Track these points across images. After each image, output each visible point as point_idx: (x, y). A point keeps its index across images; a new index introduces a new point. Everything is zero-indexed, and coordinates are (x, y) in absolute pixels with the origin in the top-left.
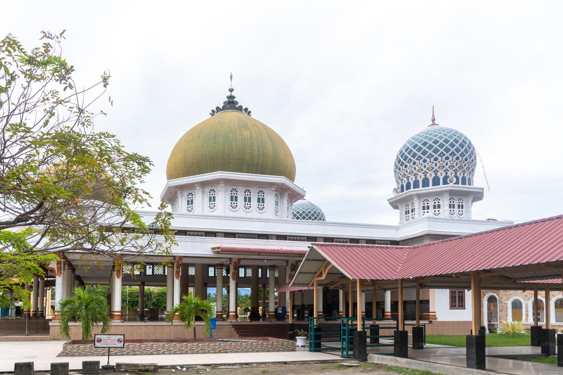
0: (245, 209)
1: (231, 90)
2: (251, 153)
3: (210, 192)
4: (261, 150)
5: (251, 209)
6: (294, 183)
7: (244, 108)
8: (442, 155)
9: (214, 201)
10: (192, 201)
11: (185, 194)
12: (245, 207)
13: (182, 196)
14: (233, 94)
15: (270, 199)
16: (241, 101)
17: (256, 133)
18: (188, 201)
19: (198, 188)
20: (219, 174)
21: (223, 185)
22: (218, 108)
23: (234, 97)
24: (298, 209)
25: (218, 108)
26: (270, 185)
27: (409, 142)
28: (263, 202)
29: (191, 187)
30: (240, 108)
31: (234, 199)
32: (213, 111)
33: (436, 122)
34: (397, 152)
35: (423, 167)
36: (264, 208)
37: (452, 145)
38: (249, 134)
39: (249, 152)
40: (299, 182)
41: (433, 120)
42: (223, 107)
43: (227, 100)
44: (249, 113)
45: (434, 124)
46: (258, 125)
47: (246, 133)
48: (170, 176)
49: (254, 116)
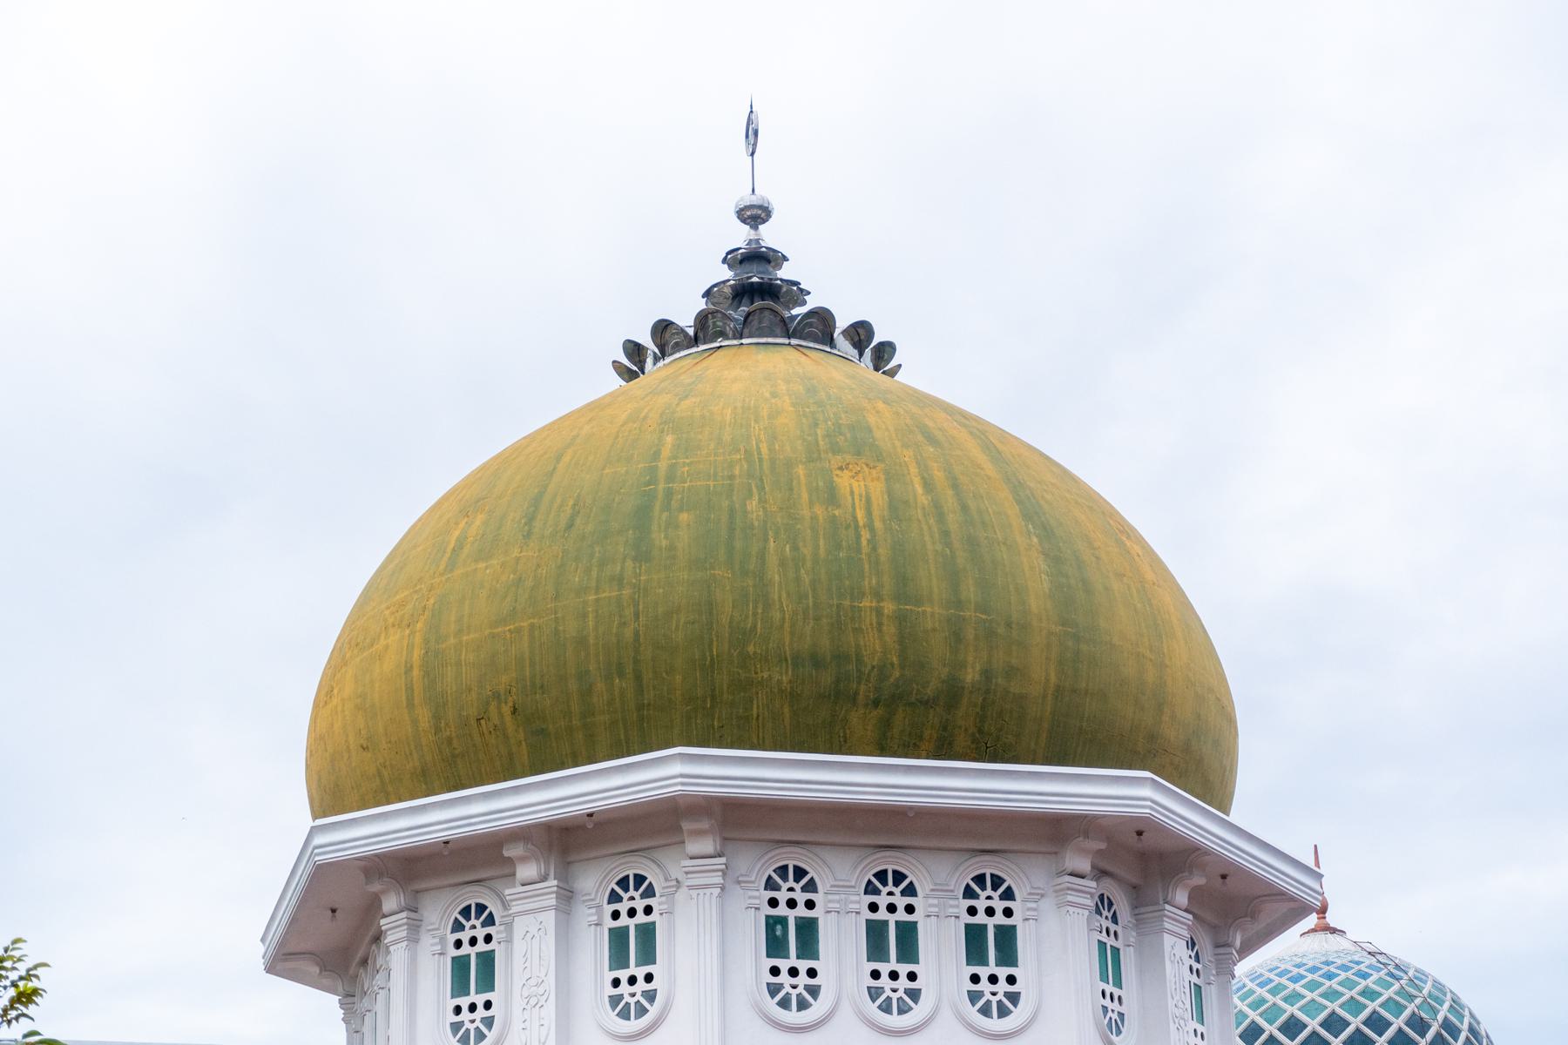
0: (771, 1005)
2: (901, 619)
3: (614, 898)
4: (970, 591)
5: (919, 1012)
6: (1234, 817)
7: (842, 323)
9: (647, 955)
10: (487, 960)
11: (439, 912)
12: (874, 993)
13: (415, 929)
14: (770, 235)
15: (1058, 936)
16: (822, 277)
17: (928, 485)
18: (460, 965)
19: (527, 871)
20: (677, 768)
21: (707, 845)
22: (663, 329)
24: (1292, 998)
25: (663, 329)
26: (1053, 832)
28: (1008, 954)
29: (480, 858)
30: (819, 327)
31: (794, 939)
32: (635, 350)
38: (877, 490)
39: (889, 607)
40: (1268, 809)
42: (702, 319)
43: (726, 274)
44: (883, 354)
46: (933, 423)
47: (859, 487)
48: (333, 793)
49: (916, 369)
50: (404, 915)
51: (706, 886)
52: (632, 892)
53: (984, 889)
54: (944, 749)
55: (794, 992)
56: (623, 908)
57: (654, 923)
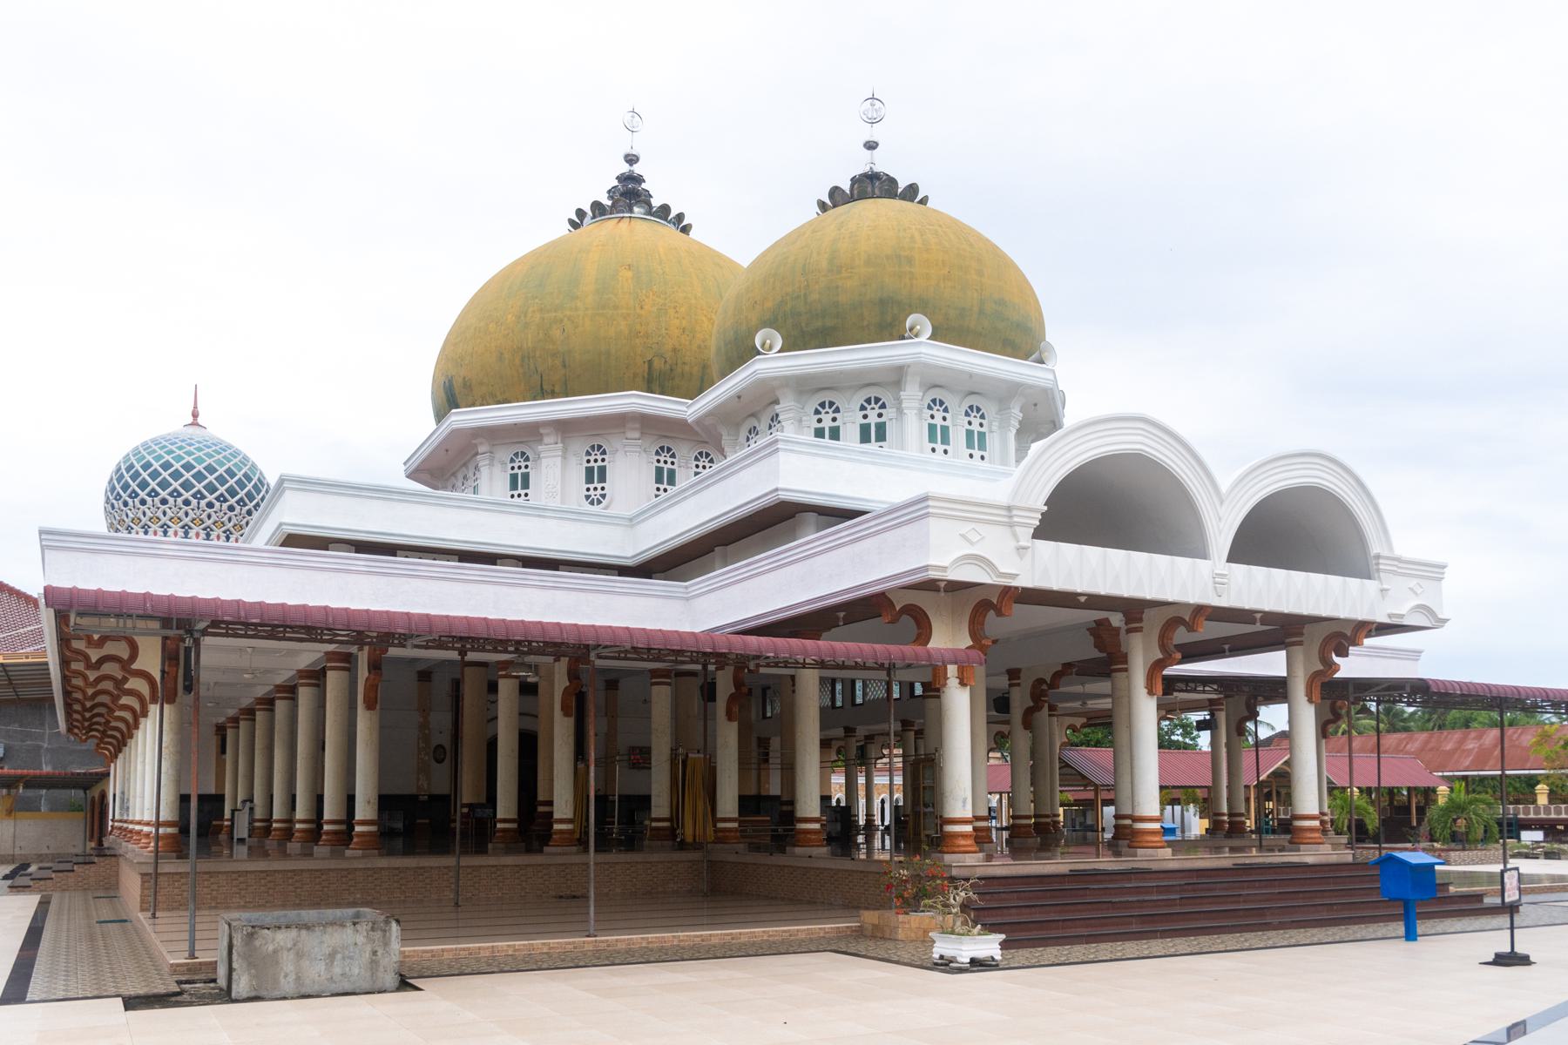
1: (631, 159)
8: (175, 494)
11: (504, 454)
14: (638, 169)
23: (639, 180)
24: (170, 452)
27: (136, 452)
29: (531, 432)
32: (580, 213)
33: (199, 420)
34: (112, 468)
35: (160, 514)
37: (199, 477)
41: (195, 415)
44: (685, 230)
45: (195, 424)
48: (449, 397)
54: (606, 389)
56: (592, 458)
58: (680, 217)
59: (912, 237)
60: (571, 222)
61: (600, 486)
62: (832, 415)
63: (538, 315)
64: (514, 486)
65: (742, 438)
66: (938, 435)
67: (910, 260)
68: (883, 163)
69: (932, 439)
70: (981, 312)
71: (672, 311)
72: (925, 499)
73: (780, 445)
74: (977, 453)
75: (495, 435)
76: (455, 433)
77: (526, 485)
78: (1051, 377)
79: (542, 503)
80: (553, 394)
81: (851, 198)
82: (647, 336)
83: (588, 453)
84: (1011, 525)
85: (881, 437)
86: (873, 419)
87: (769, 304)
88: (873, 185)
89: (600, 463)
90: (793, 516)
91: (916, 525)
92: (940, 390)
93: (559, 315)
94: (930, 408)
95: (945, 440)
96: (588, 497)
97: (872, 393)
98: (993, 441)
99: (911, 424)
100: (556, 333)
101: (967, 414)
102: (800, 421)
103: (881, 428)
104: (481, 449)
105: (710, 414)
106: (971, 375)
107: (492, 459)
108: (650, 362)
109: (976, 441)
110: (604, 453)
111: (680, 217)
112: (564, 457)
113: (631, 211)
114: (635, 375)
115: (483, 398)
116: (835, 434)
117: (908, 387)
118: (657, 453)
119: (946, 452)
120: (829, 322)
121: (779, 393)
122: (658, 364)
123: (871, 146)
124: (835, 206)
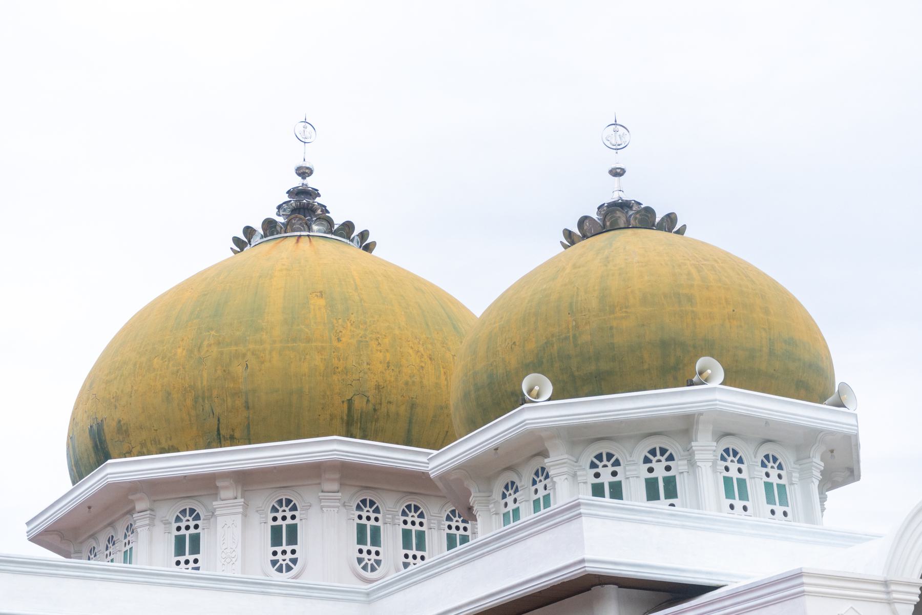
0: (359, 568)
11: (168, 512)
14: (311, 182)
19: (229, 493)
20: (335, 447)
23: (314, 193)
29: (207, 484)
31: (367, 536)
36: (378, 562)
43: (286, 198)
48: (94, 446)
49: (698, 228)
50: (148, 512)
51: (334, 507)
52: (284, 508)
53: (366, 507)
55: (370, 563)
56: (279, 515)
57: (296, 525)
58: (364, 235)
59: (689, 274)
60: (236, 241)
61: (289, 549)
62: (611, 469)
63: (215, 350)
64: (180, 550)
65: (497, 495)
66: (735, 489)
67: (690, 299)
68: (629, 190)
69: (729, 494)
70: (772, 353)
71: (373, 344)
72: (799, 575)
73: (583, 510)
74: (779, 509)
75: (157, 489)
76: (110, 488)
77: (195, 549)
78: (853, 422)
79: (219, 573)
80: (233, 440)
81: (604, 229)
82: (346, 371)
83: (274, 509)
84: (890, 602)
85: (671, 492)
86: (660, 473)
87: (531, 346)
88: (620, 215)
89: (289, 521)
90: (589, 589)
91: (789, 605)
92: (733, 439)
93: (241, 349)
94: (723, 458)
95: (744, 496)
96: (274, 563)
97: (657, 443)
98: (795, 494)
99: (704, 477)
100: (237, 369)
101: (763, 465)
102: (575, 476)
103: (670, 483)
104: (139, 506)
105: (462, 467)
106: (767, 422)
107: (152, 518)
108: (350, 401)
109: (776, 494)
110: (294, 508)
111: (364, 235)
112: (245, 515)
113: (310, 229)
114: (332, 417)
115: (143, 445)
116: (617, 491)
117: (700, 436)
118: (359, 508)
119: (745, 508)
120: (604, 366)
121: (548, 445)
122: (359, 404)
123: (617, 173)
124: (585, 237)
